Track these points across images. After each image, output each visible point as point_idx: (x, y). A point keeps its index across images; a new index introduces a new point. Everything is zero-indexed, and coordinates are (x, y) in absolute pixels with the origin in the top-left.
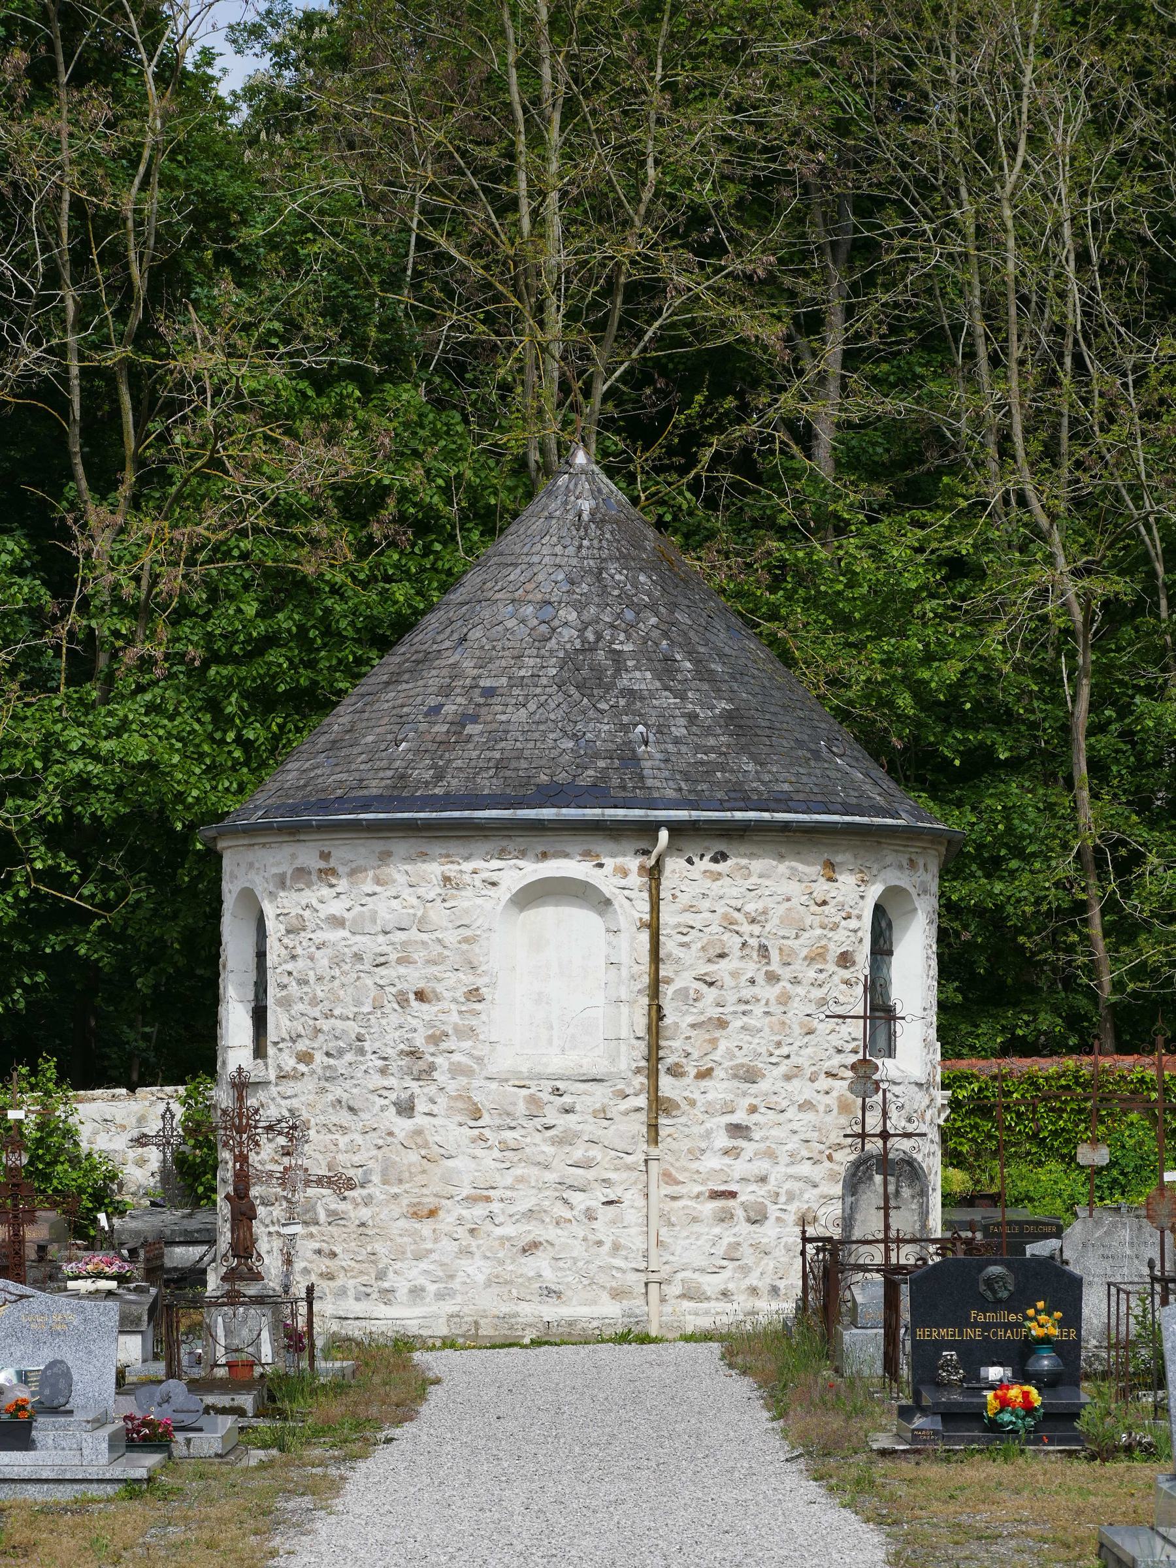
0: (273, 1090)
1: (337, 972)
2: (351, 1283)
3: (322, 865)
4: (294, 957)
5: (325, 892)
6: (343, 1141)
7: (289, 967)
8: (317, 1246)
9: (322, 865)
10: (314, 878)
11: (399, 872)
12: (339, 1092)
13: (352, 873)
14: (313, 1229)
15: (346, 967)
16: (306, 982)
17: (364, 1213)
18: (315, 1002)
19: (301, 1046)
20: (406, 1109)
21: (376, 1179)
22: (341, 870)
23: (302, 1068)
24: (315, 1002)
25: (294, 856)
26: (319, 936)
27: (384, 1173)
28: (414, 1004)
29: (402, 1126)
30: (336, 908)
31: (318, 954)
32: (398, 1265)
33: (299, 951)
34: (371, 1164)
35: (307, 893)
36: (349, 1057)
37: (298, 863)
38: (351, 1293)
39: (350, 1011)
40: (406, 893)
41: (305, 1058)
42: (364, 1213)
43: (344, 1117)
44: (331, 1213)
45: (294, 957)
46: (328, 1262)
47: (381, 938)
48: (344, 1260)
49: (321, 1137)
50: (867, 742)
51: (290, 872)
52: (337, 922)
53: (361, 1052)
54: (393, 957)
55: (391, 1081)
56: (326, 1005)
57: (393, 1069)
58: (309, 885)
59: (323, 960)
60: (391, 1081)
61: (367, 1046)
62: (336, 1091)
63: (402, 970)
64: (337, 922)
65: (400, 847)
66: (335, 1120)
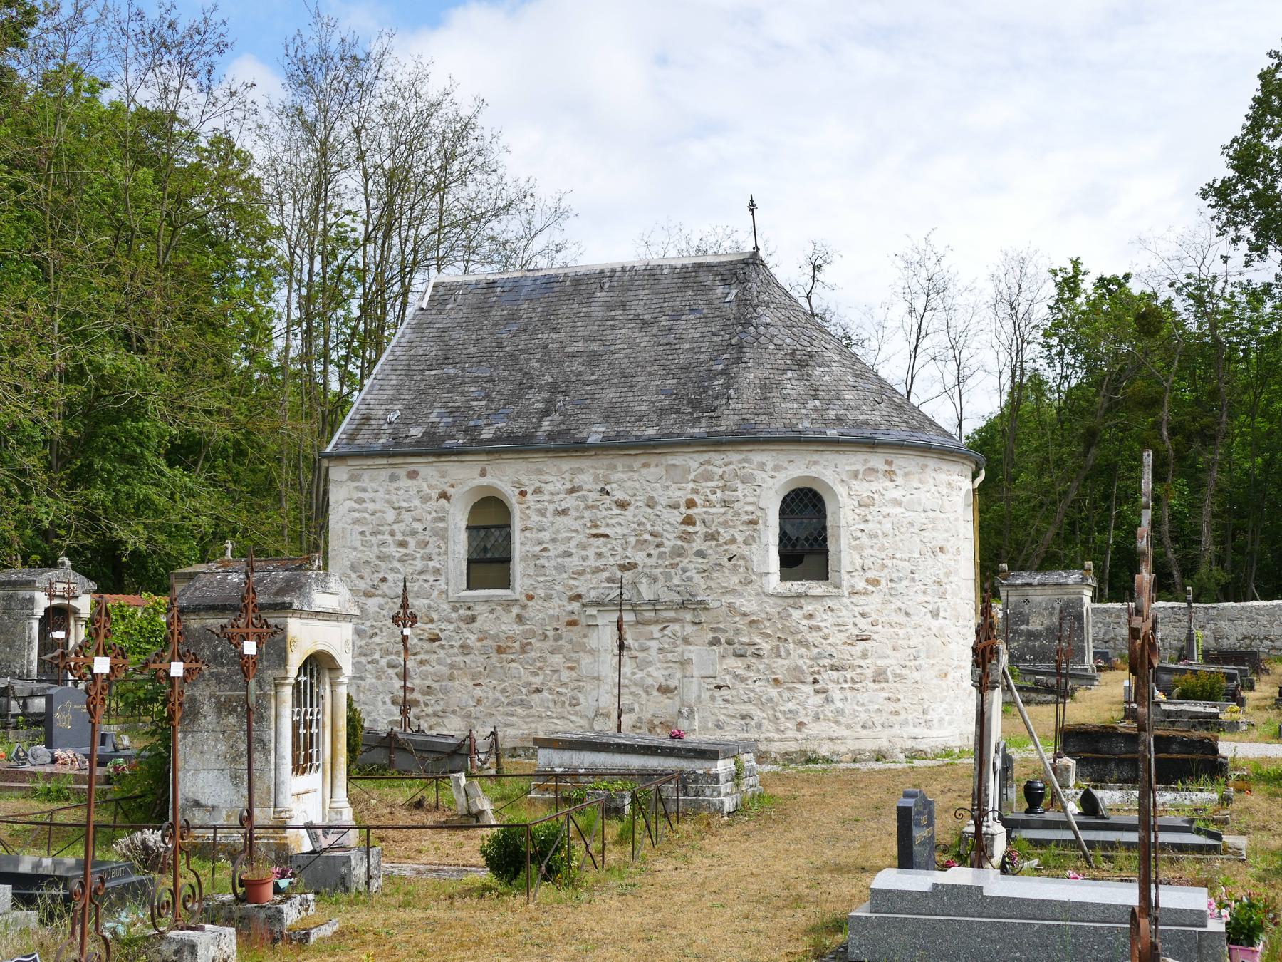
0: (846, 601)
1: (896, 532)
2: (910, 717)
3: (887, 468)
4: (866, 521)
5: (888, 484)
6: (901, 632)
7: (862, 527)
8: (887, 695)
9: (887, 468)
10: (880, 475)
11: (930, 475)
12: (899, 604)
13: (906, 474)
14: (884, 685)
15: (903, 530)
16: (876, 537)
17: (917, 675)
18: (883, 548)
19: (870, 575)
20: (935, 614)
21: (923, 655)
22: (898, 472)
23: (870, 588)
24: (883, 548)
25: (866, 461)
26: (885, 510)
27: (927, 651)
28: (530, 603)
29: (935, 624)
30: (896, 494)
31: (884, 521)
32: (934, 706)
33: (869, 517)
34: (920, 647)
35: (875, 483)
36: (905, 583)
37: (870, 465)
38: (911, 723)
39: (906, 556)
40: (933, 489)
41: (876, 582)
42: (917, 675)
43: (901, 618)
44: (895, 675)
45: (866, 521)
46: (894, 704)
47: (923, 515)
48: (904, 703)
49: (885, 629)
50: (322, 528)
51: (862, 470)
52: (897, 503)
53: (913, 580)
54: (930, 526)
55: (928, 598)
56: (890, 552)
57: (929, 591)
58: (877, 479)
59: (887, 526)
60: (928, 598)
61: (916, 576)
62: (897, 603)
63: (934, 534)
64: (897, 503)
65: (932, 463)
66: (896, 619)
